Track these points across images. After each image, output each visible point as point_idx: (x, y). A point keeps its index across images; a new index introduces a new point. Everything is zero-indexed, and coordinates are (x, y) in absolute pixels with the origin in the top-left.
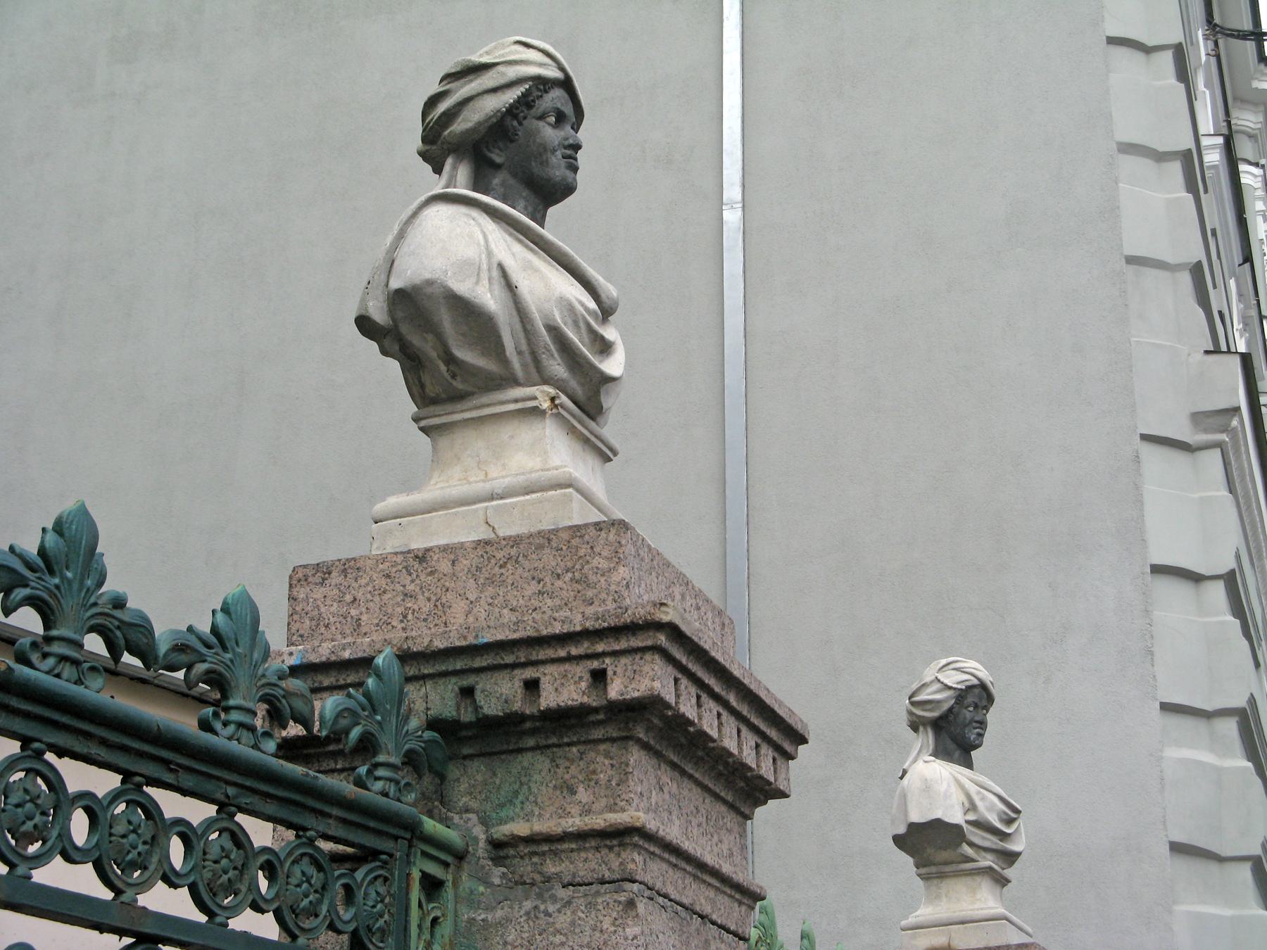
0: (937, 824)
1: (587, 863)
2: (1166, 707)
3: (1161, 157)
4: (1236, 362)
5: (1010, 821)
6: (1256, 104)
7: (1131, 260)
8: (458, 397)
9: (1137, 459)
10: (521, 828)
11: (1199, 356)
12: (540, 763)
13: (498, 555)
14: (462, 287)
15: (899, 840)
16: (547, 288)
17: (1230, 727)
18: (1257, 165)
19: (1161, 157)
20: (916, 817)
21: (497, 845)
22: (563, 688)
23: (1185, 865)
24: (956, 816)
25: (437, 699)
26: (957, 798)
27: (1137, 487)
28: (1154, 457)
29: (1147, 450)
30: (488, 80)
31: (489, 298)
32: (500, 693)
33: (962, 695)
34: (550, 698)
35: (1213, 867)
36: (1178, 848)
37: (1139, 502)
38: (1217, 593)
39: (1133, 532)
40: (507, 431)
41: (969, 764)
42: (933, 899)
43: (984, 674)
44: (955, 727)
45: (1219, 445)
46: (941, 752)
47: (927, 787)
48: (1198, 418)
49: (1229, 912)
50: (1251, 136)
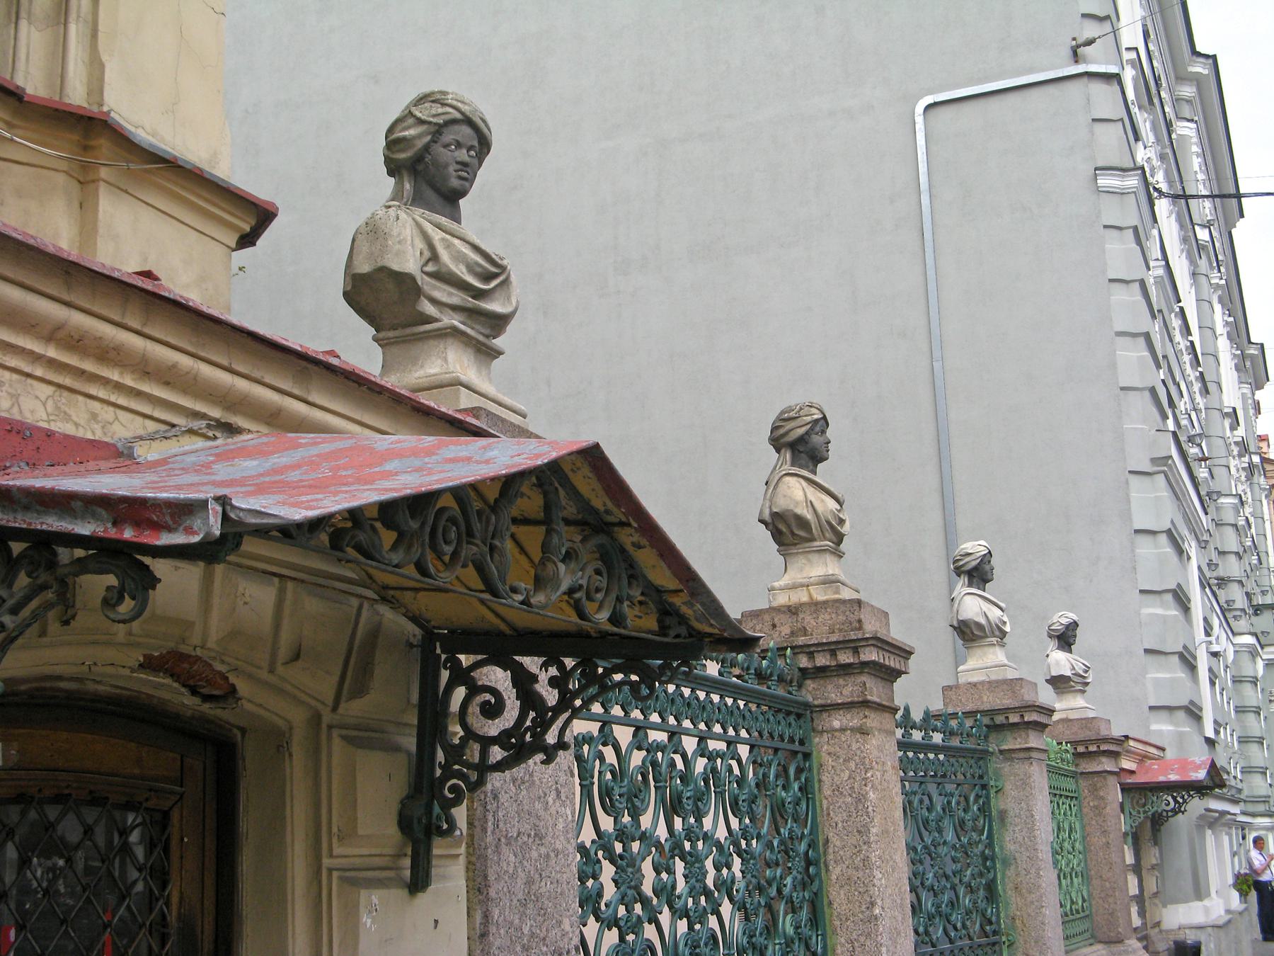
0: (1062, 676)
1: (1022, 755)
2: (1142, 591)
3: (1134, 335)
4: (1171, 435)
5: (1086, 672)
6: (1191, 80)
7: (1122, 389)
8: (973, 640)
9: (1127, 482)
10: (1006, 747)
11: (1153, 432)
12: (1008, 733)
13: (993, 685)
14: (976, 619)
15: (1047, 681)
16: (994, 614)
17: (1169, 597)
18: (1192, 120)
19: (1134, 335)
20: (1054, 674)
21: (1001, 752)
22: (1014, 719)
23: (1150, 658)
24: (1068, 673)
25: (986, 721)
26: (1068, 666)
27: (1128, 495)
28: (1134, 480)
29: (1133, 478)
30: (972, 557)
31: (983, 621)
32: (1000, 719)
33: (1068, 627)
34: (1011, 721)
35: (1162, 658)
36: (1147, 651)
37: (1129, 501)
38: (1163, 539)
39: (1127, 515)
40: (986, 649)
41: (1070, 652)
42: (1061, 701)
43: (1075, 618)
44: (1065, 639)
45: (1164, 472)
46: (1061, 648)
47: (1058, 663)
48: (1154, 461)
49: (1168, 676)
50: (1187, 101)
